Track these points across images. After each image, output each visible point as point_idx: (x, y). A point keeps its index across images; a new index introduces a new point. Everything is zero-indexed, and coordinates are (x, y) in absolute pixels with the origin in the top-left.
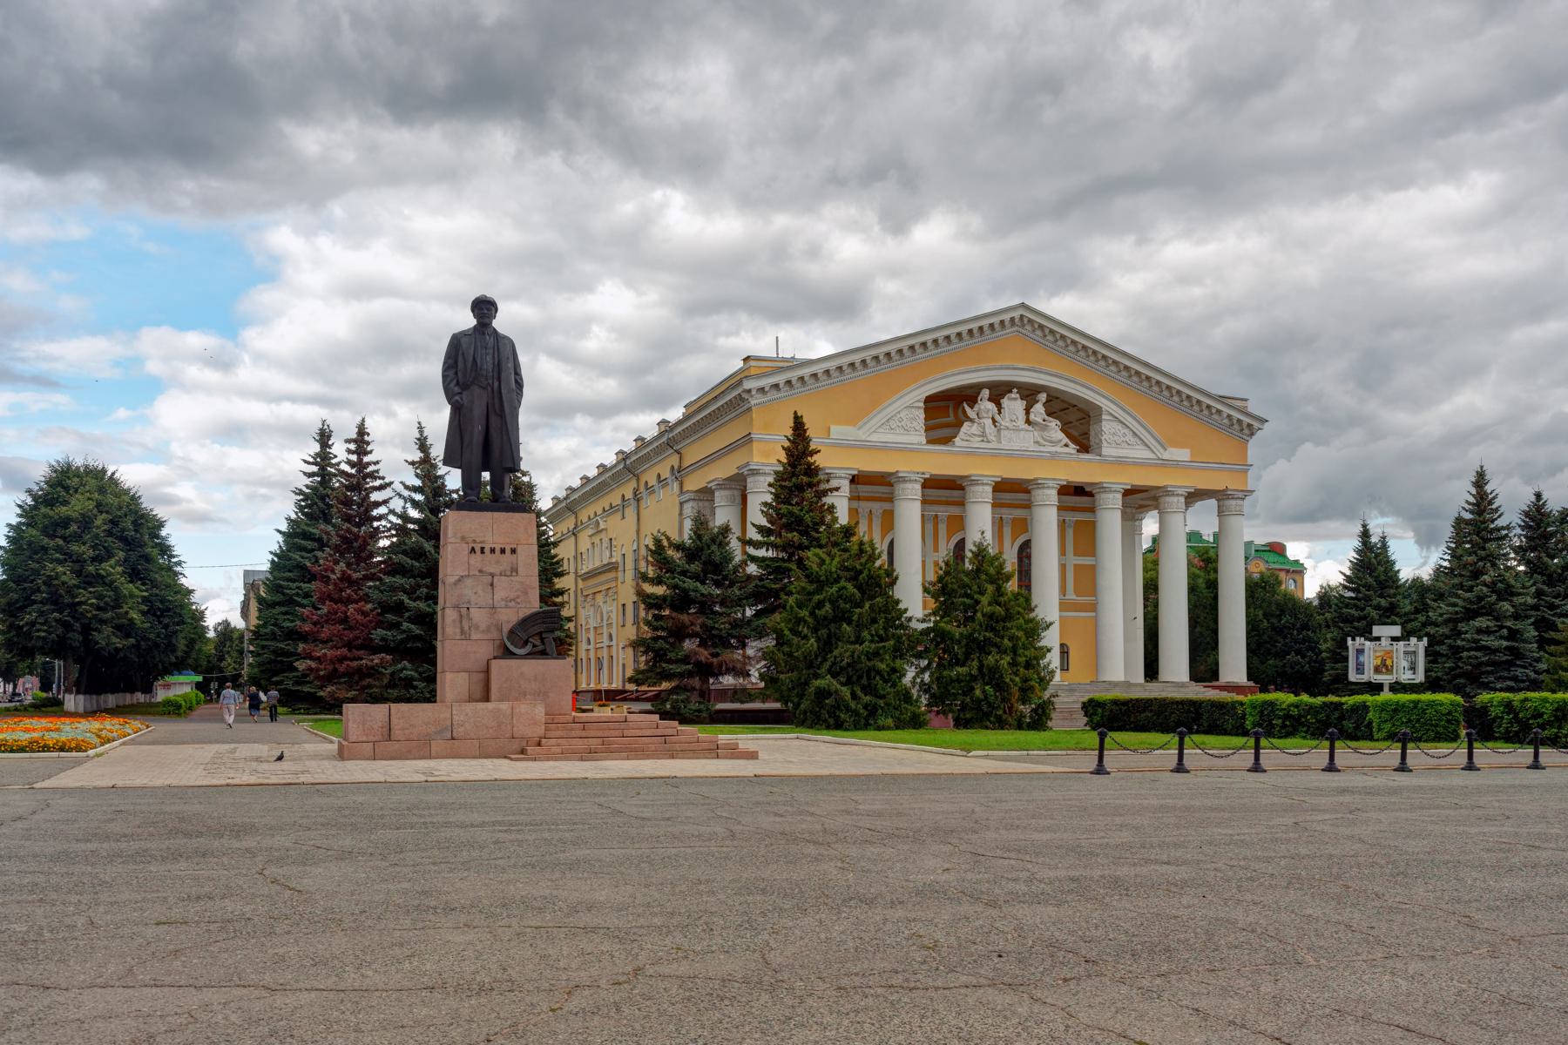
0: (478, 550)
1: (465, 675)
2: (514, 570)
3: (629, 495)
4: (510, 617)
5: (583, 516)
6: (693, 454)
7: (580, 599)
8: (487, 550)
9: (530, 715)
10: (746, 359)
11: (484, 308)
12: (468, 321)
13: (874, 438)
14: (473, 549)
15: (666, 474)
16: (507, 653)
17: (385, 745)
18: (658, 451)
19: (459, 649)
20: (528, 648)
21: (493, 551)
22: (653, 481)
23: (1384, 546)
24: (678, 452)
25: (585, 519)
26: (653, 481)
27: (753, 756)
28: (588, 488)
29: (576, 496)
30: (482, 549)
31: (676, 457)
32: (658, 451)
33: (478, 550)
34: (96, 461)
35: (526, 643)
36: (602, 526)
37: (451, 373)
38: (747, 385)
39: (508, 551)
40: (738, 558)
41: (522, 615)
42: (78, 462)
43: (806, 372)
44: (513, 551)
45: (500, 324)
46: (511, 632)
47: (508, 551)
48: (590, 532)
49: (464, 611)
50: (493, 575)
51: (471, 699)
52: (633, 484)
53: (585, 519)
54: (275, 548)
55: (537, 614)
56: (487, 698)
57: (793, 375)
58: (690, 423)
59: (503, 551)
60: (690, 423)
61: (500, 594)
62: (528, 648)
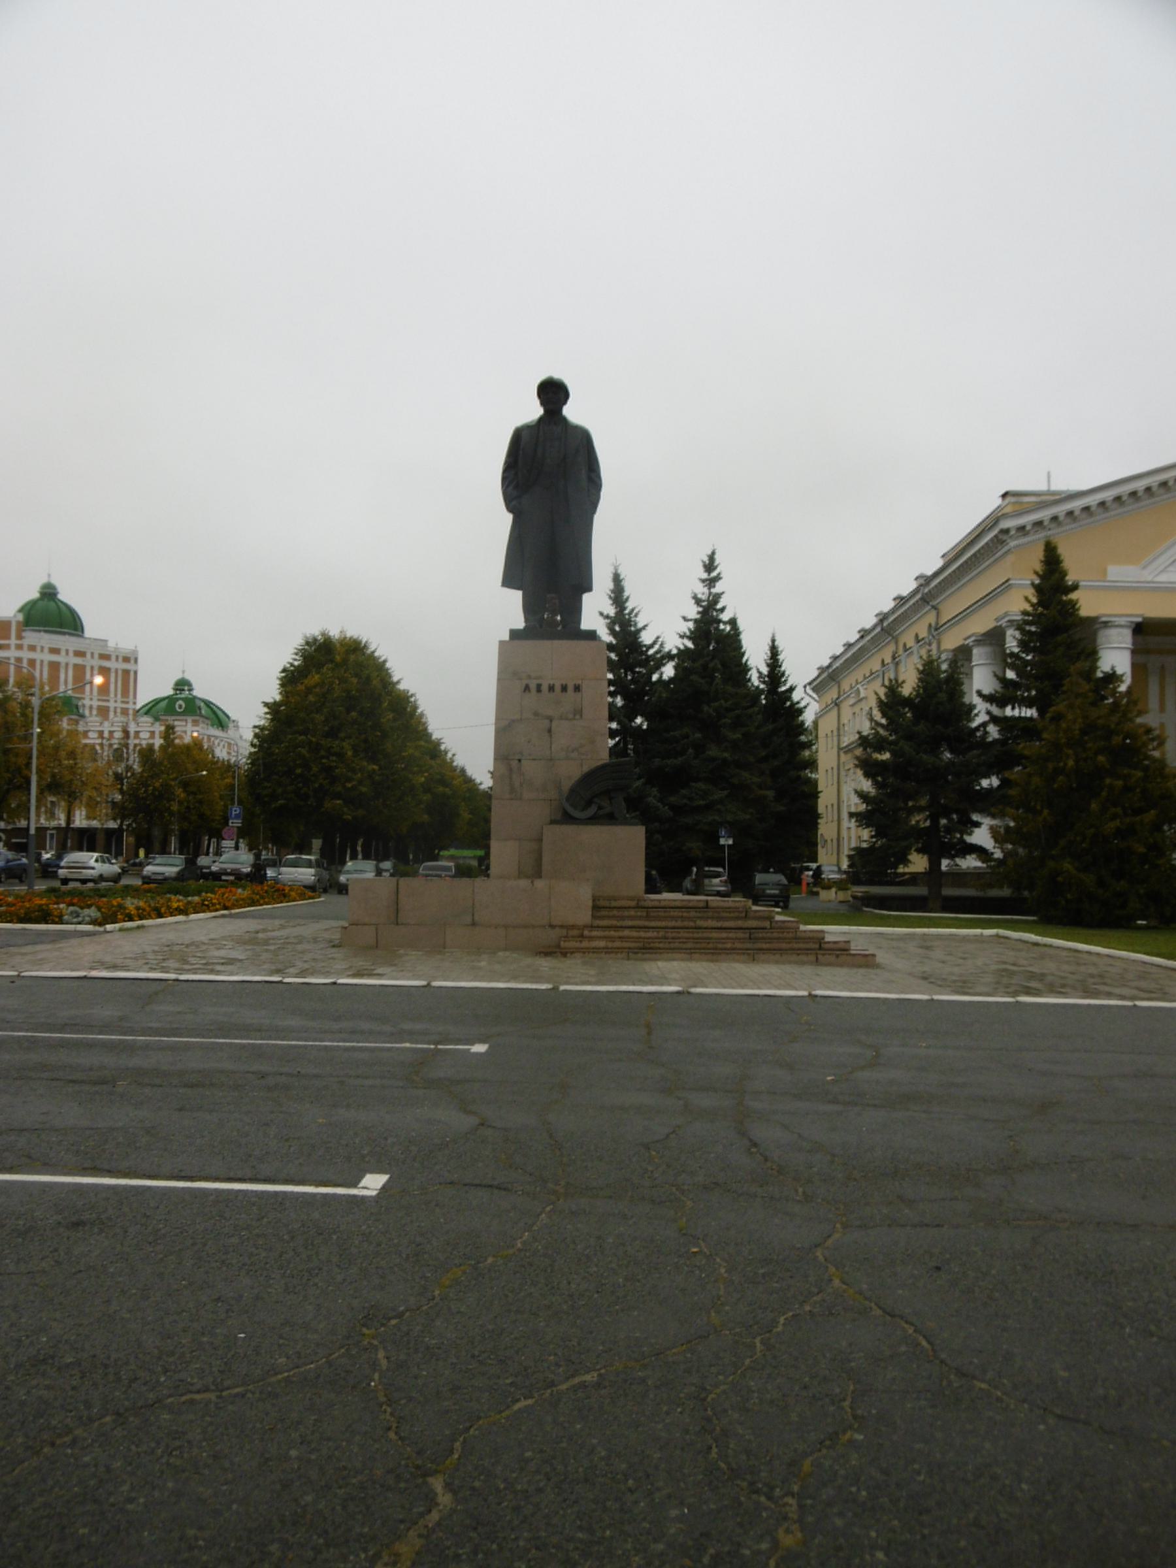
0: (533, 686)
2: (578, 712)
3: (888, 660)
4: (571, 772)
5: (845, 685)
6: (952, 607)
7: (843, 773)
8: (545, 688)
10: (1005, 496)
11: (553, 393)
12: (533, 411)
13: (1163, 578)
14: (527, 688)
15: (923, 634)
16: (567, 818)
18: (915, 608)
20: (592, 811)
21: (551, 688)
22: (911, 643)
24: (934, 607)
25: (847, 689)
26: (911, 643)
27: (867, 961)
28: (849, 654)
29: (837, 664)
30: (539, 688)
31: (934, 613)
32: (915, 608)
33: (533, 686)
34: (352, 632)
35: (589, 803)
36: (862, 695)
38: (1005, 524)
39: (570, 688)
40: (982, 718)
42: (334, 633)
43: (1077, 505)
44: (577, 688)
45: (572, 412)
46: (573, 791)
47: (570, 688)
48: (852, 701)
49: (514, 763)
51: (521, 874)
52: (892, 648)
53: (847, 689)
55: (603, 767)
56: (537, 873)
57: (1061, 510)
58: (950, 571)
59: (564, 688)
60: (950, 571)
62: (592, 811)
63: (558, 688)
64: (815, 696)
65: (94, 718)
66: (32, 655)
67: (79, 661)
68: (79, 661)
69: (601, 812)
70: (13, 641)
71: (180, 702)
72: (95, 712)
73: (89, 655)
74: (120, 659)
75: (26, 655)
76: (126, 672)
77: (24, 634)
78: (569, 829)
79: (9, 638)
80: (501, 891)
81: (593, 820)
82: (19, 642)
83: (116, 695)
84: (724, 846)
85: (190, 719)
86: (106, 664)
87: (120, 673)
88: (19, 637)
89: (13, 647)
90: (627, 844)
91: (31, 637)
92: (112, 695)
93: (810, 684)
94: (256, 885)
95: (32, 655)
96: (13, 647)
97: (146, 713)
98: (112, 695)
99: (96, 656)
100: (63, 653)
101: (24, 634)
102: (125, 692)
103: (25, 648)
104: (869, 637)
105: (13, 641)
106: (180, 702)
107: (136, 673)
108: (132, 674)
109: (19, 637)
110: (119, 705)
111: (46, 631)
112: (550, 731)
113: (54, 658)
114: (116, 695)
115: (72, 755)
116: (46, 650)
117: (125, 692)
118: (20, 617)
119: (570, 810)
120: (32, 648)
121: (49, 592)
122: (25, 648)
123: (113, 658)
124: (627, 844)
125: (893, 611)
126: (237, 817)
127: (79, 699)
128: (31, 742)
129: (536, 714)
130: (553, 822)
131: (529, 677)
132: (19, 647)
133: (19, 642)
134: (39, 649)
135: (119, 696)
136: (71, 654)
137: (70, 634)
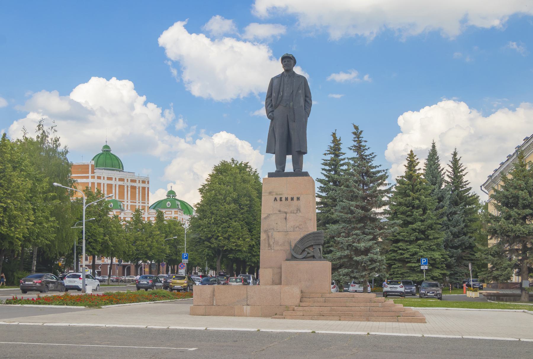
0: (278, 199)
1: (270, 270)
2: (298, 210)
4: (295, 237)
8: (283, 199)
9: (291, 293)
16: (293, 258)
17: (212, 309)
19: (270, 255)
23: (26, 139)
27: (422, 321)
30: (281, 198)
33: (278, 199)
37: (269, 100)
39: (295, 199)
41: (302, 235)
44: (298, 199)
50: (286, 213)
54: (199, 202)
55: (314, 233)
56: (280, 283)
59: (292, 199)
61: (291, 223)
63: (289, 199)
64: (486, 191)
65: (128, 211)
66: (99, 181)
67: (121, 183)
68: (121, 183)
69: (309, 255)
70: (90, 175)
71: (169, 202)
72: (129, 208)
73: (126, 181)
74: (141, 182)
75: (96, 181)
76: (144, 188)
77: (95, 171)
78: (294, 263)
79: (88, 173)
80: (263, 289)
81: (305, 258)
82: (93, 175)
83: (139, 200)
84: (423, 270)
85: (173, 211)
86: (134, 184)
87: (141, 189)
88: (93, 172)
89: (90, 177)
90: (323, 268)
91: (98, 172)
92: (137, 200)
93: (483, 185)
94: (186, 292)
95: (99, 181)
96: (90, 177)
97: (154, 209)
98: (137, 200)
99: (129, 180)
100: (114, 179)
101: (95, 171)
102: (143, 198)
103: (96, 178)
104: (511, 160)
105: (90, 175)
106: (169, 202)
107: (148, 188)
108: (146, 189)
109: (93, 172)
110: (141, 204)
111: (105, 169)
112: (286, 219)
113: (110, 182)
114: (139, 200)
115: (175, 224)
116: (106, 179)
117: (143, 198)
118: (93, 163)
119: (295, 255)
120: (99, 178)
121: (107, 150)
122: (96, 178)
123: (137, 181)
124: (323, 268)
125: (523, 145)
126: (186, 258)
127: (121, 202)
128: (83, 226)
129: (280, 211)
130: (287, 260)
131: (277, 194)
132: (93, 177)
133: (93, 175)
134: (102, 178)
135: (141, 200)
136: (117, 180)
137: (117, 170)
